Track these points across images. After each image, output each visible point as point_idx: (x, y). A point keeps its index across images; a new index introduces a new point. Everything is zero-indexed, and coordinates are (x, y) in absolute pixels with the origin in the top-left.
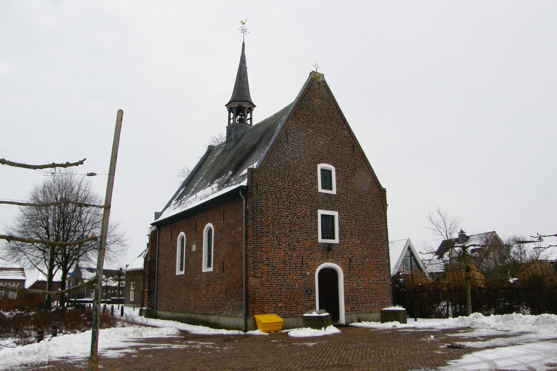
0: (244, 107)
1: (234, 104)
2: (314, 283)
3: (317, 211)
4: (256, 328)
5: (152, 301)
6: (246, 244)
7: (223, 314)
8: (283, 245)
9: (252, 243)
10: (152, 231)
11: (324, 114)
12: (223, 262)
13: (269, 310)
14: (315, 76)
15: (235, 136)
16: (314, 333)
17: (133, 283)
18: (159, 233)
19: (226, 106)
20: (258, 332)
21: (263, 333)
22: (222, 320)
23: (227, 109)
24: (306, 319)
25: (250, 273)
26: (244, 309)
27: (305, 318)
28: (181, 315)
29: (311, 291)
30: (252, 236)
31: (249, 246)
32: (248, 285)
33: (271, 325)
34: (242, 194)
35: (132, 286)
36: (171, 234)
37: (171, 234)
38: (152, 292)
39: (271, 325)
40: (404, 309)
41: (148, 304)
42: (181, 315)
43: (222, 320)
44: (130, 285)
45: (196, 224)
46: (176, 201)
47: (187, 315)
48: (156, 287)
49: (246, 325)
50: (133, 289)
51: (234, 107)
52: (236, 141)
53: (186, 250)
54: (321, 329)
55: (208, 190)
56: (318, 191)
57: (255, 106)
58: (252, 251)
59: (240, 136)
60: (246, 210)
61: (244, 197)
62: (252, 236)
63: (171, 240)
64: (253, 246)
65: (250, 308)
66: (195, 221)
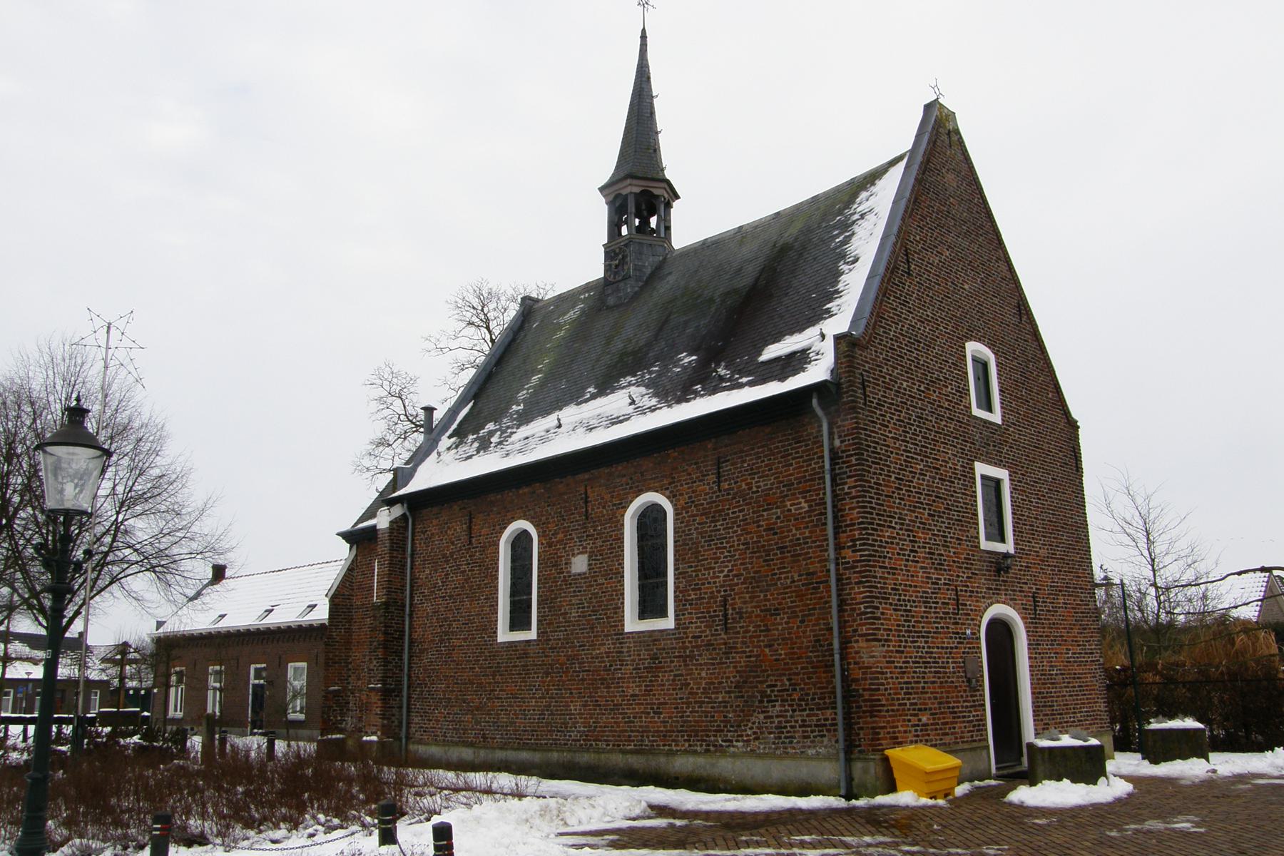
0: (657, 197)
1: (630, 185)
2: (979, 658)
3: (973, 465)
4: (892, 788)
5: (393, 718)
6: (839, 547)
7: (732, 749)
8: (921, 554)
9: (860, 545)
10: (392, 517)
11: (965, 214)
12: (725, 601)
13: (905, 735)
14: (941, 113)
15: (637, 268)
16: (1087, 794)
17: (218, 668)
18: (414, 525)
19: (602, 189)
20: (905, 797)
21: (925, 801)
22: (725, 766)
23: (604, 200)
24: (1050, 755)
25: (855, 631)
26: (841, 734)
27: (1047, 751)
28: (524, 755)
29: (977, 681)
30: (859, 523)
31: (848, 553)
32: (849, 664)
33: (940, 777)
34: (820, 404)
35: (211, 679)
36: (470, 528)
37: (470, 528)
38: (393, 690)
39: (940, 777)
40: (1201, 726)
41: (383, 726)
42: (524, 755)
43: (725, 766)
44: (207, 674)
45: (587, 497)
46: (453, 440)
47: (566, 756)
48: (406, 678)
49: (850, 779)
50: (218, 685)
51: (631, 193)
52: (641, 284)
53: (540, 571)
54: (1095, 784)
55: (616, 402)
56: (971, 412)
57: (677, 197)
58: (862, 566)
59: (648, 271)
60: (832, 450)
61: (826, 414)
62: (859, 523)
63: (470, 543)
64: (867, 553)
65: (861, 728)
66: (582, 490)
